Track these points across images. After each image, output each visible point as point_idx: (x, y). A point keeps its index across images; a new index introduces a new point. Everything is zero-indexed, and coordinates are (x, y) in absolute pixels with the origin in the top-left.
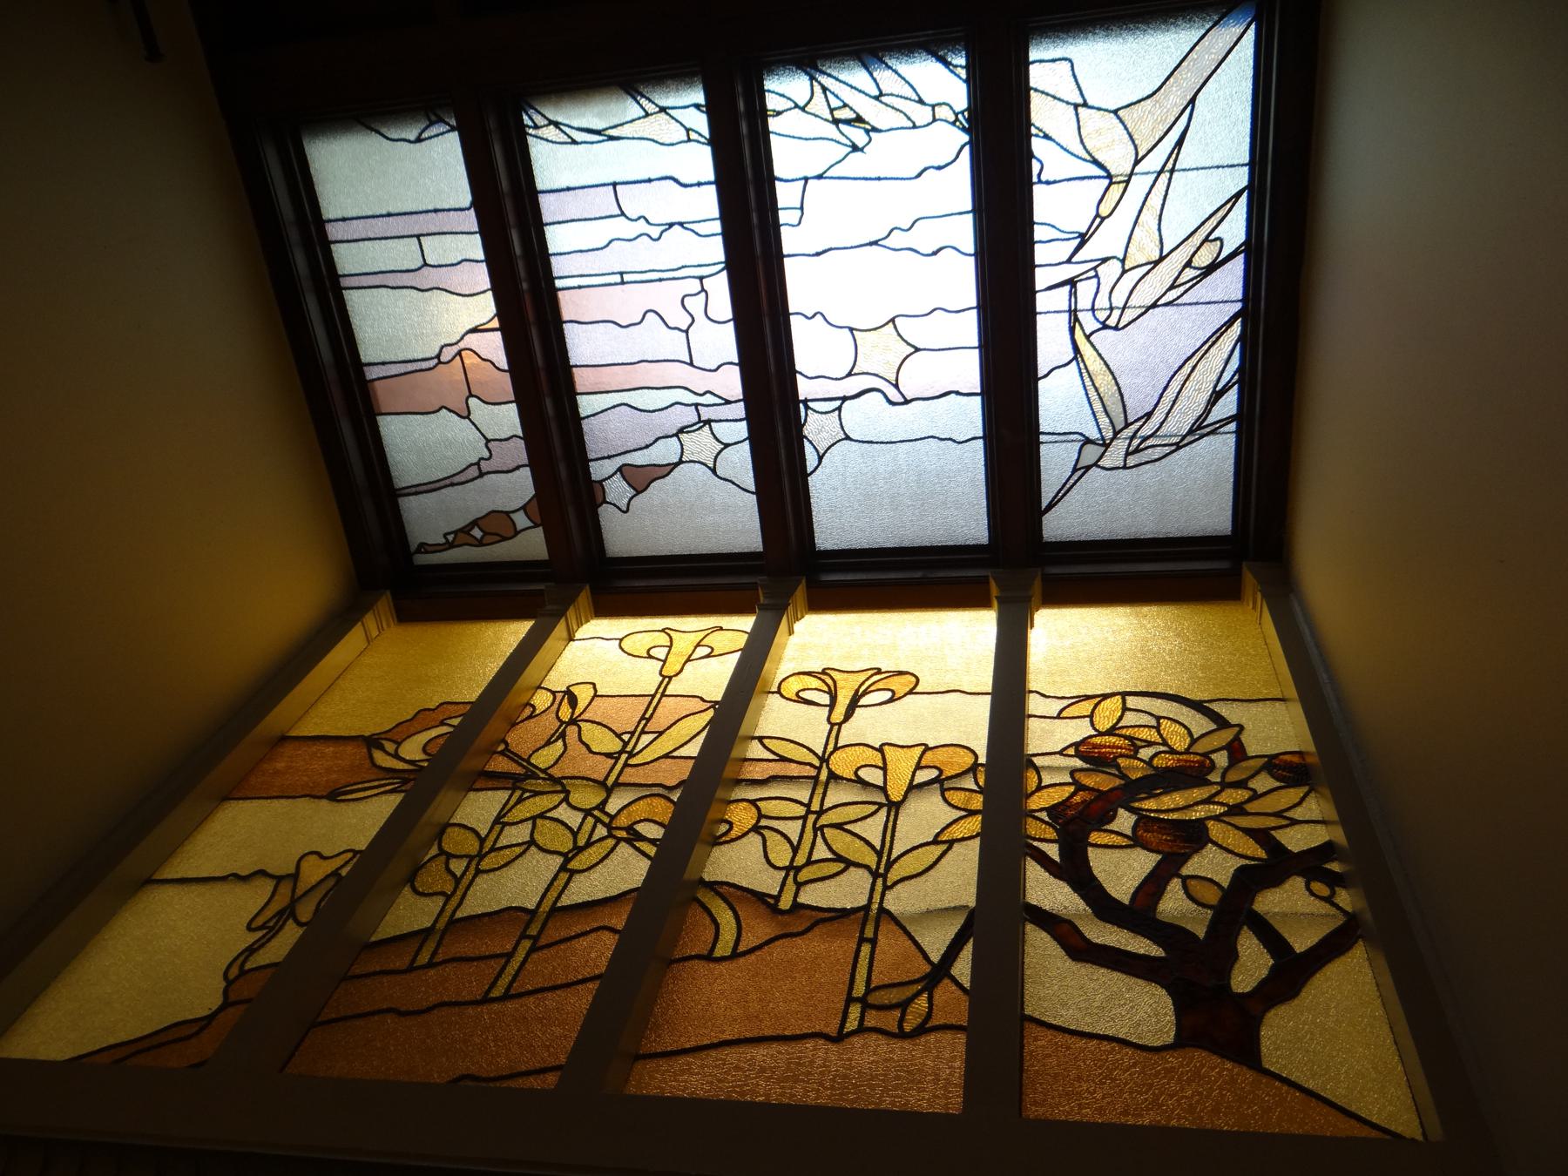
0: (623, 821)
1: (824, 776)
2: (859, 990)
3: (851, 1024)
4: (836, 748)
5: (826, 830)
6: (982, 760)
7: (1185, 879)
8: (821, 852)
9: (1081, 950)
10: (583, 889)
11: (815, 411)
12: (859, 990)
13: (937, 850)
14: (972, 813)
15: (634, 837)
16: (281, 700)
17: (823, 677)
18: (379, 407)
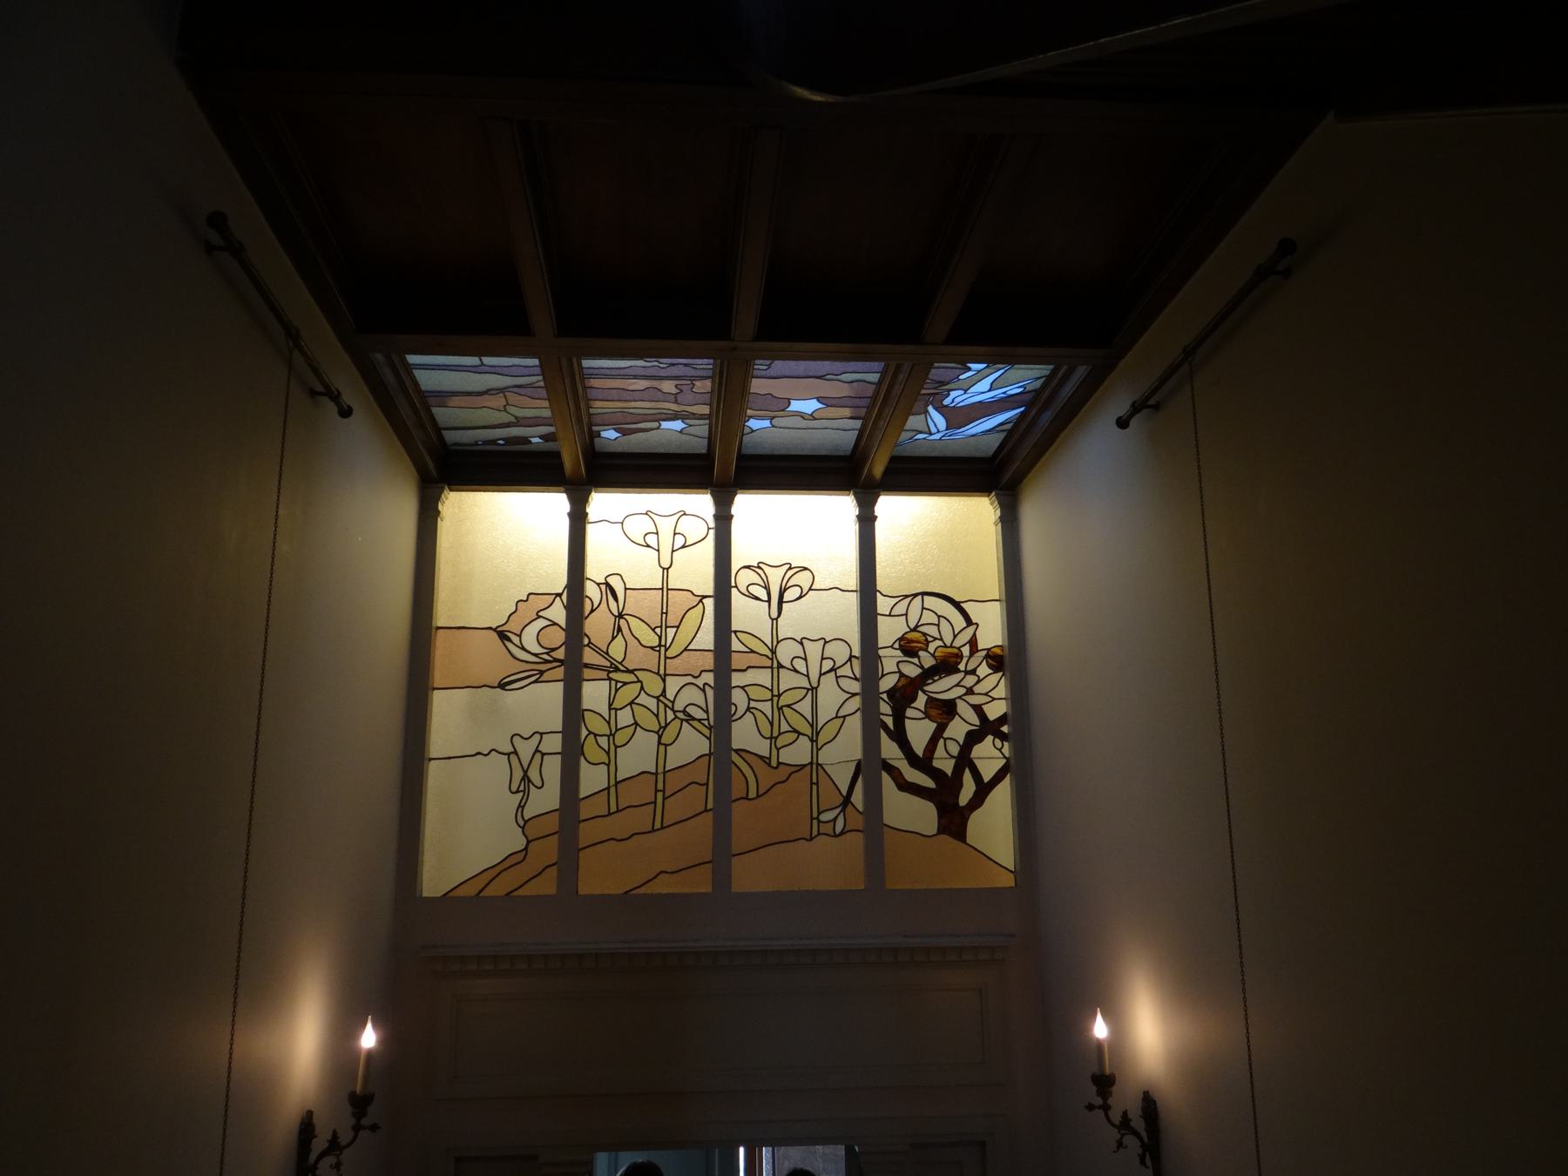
0: (679, 706)
1: (775, 665)
2: (815, 815)
3: (815, 832)
4: (778, 642)
5: (784, 708)
6: (856, 652)
7: (945, 739)
8: (785, 727)
9: (905, 786)
10: (676, 757)
11: (920, 710)
12: (815, 815)
13: (842, 713)
14: (854, 695)
15: (690, 718)
16: (434, 586)
17: (757, 570)
18: (1007, 704)
